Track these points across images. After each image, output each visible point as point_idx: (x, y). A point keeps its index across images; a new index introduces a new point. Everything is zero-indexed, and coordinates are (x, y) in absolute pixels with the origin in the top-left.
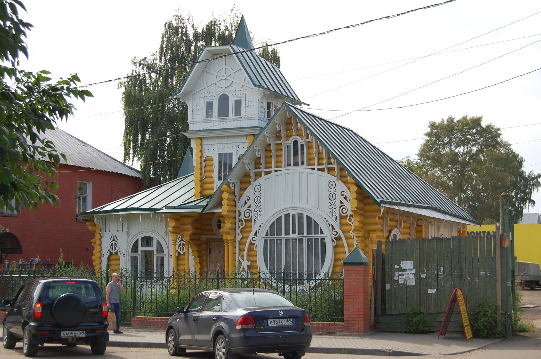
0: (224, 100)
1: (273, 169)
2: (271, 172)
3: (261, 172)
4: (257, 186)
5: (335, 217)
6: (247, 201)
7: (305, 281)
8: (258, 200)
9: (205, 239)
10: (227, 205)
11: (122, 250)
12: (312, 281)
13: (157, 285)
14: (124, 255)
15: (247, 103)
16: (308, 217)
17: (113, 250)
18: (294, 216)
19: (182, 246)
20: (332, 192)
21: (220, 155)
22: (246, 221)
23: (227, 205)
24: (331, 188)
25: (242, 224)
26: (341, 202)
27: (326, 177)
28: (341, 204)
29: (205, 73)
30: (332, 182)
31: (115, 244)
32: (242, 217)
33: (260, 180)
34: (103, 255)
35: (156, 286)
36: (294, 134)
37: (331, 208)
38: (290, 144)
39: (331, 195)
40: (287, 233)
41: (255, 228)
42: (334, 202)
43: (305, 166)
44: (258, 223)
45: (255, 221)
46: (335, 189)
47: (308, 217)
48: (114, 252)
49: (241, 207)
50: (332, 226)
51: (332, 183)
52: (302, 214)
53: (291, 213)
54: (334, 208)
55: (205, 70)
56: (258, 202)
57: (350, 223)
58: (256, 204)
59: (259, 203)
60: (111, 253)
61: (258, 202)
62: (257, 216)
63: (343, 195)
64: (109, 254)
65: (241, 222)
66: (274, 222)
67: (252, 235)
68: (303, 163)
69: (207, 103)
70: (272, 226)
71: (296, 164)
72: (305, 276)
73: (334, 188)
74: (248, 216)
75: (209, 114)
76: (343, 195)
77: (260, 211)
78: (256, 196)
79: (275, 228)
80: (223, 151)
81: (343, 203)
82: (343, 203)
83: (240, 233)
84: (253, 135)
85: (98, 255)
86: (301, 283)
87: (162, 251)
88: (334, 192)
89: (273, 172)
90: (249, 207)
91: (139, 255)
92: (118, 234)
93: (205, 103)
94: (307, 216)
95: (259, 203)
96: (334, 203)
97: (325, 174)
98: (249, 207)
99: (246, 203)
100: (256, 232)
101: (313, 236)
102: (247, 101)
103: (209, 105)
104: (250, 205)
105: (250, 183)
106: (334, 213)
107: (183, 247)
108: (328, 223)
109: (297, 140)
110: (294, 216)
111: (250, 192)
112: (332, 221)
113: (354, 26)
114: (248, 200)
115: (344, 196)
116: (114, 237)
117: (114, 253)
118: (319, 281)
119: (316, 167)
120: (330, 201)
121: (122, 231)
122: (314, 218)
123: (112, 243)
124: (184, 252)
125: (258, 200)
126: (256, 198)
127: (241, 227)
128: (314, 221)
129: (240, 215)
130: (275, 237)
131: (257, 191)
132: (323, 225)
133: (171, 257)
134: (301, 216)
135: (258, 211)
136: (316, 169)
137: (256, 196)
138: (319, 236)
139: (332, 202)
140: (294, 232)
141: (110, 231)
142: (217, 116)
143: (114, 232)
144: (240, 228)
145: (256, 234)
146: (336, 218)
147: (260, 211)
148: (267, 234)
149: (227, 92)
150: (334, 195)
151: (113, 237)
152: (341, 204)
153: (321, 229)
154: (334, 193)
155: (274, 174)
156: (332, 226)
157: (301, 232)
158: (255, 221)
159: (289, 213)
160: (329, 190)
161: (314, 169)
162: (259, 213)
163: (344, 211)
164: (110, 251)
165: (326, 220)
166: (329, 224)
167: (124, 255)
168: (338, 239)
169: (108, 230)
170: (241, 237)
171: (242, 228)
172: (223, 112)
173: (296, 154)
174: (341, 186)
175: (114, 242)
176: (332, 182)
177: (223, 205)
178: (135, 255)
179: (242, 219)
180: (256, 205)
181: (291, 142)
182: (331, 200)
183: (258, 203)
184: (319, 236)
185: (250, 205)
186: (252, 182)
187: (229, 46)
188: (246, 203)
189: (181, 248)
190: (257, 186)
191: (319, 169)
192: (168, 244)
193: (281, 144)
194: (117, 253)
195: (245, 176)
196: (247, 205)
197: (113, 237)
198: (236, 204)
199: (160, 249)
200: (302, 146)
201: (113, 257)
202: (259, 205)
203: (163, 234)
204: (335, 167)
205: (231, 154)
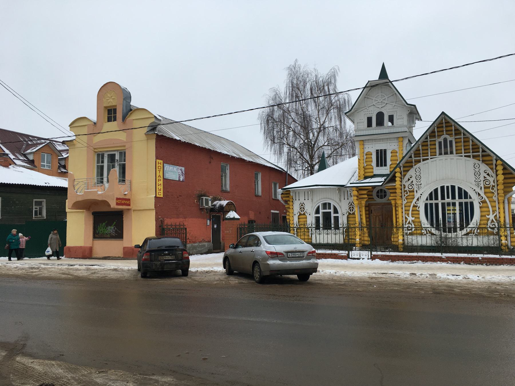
0: (380, 116)
1: (429, 157)
2: (428, 159)
3: (420, 159)
5: (481, 187)
6: (410, 178)
8: (478, 174)
9: (368, 204)
10: (502, 174)
13: (339, 233)
14: (310, 214)
17: (301, 211)
18: (448, 187)
19: (351, 208)
20: (477, 171)
21: (377, 151)
22: (410, 192)
23: (502, 174)
24: (476, 168)
26: (485, 177)
27: (471, 161)
28: (484, 178)
29: (366, 98)
32: (407, 189)
33: (419, 165)
34: (295, 215)
36: (445, 133)
37: (477, 182)
40: (443, 198)
41: (417, 196)
42: (479, 177)
43: (455, 154)
44: (420, 192)
45: (417, 191)
46: (479, 168)
48: (351, 212)
51: (477, 165)
53: (445, 185)
54: (479, 182)
56: (418, 179)
57: (493, 191)
58: (417, 180)
59: (479, 176)
60: (350, 214)
61: (477, 175)
62: (418, 188)
64: (348, 214)
67: (415, 200)
69: (368, 118)
70: (431, 194)
71: (446, 153)
72: (458, 226)
78: (475, 171)
79: (434, 195)
80: (379, 148)
81: (486, 178)
82: (486, 178)
83: (405, 199)
85: (291, 215)
86: (455, 231)
89: (429, 159)
90: (412, 182)
91: (320, 215)
93: (388, 116)
95: (479, 176)
97: (471, 159)
98: (412, 182)
99: (409, 180)
100: (418, 199)
101: (463, 200)
102: (398, 115)
103: (369, 120)
106: (479, 185)
110: (448, 187)
111: (412, 172)
112: (478, 190)
115: (487, 173)
116: (351, 203)
117: (351, 213)
118: (470, 229)
119: (463, 154)
120: (475, 177)
122: (464, 188)
123: (301, 207)
126: (417, 177)
127: (406, 195)
128: (464, 190)
129: (404, 188)
130: (434, 202)
131: (418, 172)
132: (471, 193)
134: (453, 187)
136: (463, 156)
137: (475, 171)
138: (468, 200)
140: (448, 198)
141: (299, 200)
142: (367, 127)
143: (302, 200)
144: (405, 196)
145: (418, 199)
146: (481, 188)
147: (420, 185)
148: (427, 200)
149: (383, 110)
150: (478, 173)
151: (301, 204)
152: (484, 178)
153: (470, 195)
155: (430, 160)
157: (454, 197)
158: (417, 191)
161: (462, 156)
162: (420, 186)
163: (487, 183)
166: (476, 192)
167: (310, 214)
168: (484, 202)
169: (297, 199)
172: (380, 122)
173: (446, 146)
174: (484, 167)
175: (302, 207)
177: (396, 181)
179: (406, 190)
180: (417, 181)
181: (441, 139)
182: (477, 176)
184: (468, 200)
186: (413, 166)
188: (409, 180)
189: (351, 209)
191: (465, 156)
196: (410, 181)
197: (301, 204)
198: (402, 180)
199: (336, 211)
200: (451, 142)
201: (302, 215)
202: (420, 180)
203: (338, 200)
204: (480, 155)
205: (385, 151)
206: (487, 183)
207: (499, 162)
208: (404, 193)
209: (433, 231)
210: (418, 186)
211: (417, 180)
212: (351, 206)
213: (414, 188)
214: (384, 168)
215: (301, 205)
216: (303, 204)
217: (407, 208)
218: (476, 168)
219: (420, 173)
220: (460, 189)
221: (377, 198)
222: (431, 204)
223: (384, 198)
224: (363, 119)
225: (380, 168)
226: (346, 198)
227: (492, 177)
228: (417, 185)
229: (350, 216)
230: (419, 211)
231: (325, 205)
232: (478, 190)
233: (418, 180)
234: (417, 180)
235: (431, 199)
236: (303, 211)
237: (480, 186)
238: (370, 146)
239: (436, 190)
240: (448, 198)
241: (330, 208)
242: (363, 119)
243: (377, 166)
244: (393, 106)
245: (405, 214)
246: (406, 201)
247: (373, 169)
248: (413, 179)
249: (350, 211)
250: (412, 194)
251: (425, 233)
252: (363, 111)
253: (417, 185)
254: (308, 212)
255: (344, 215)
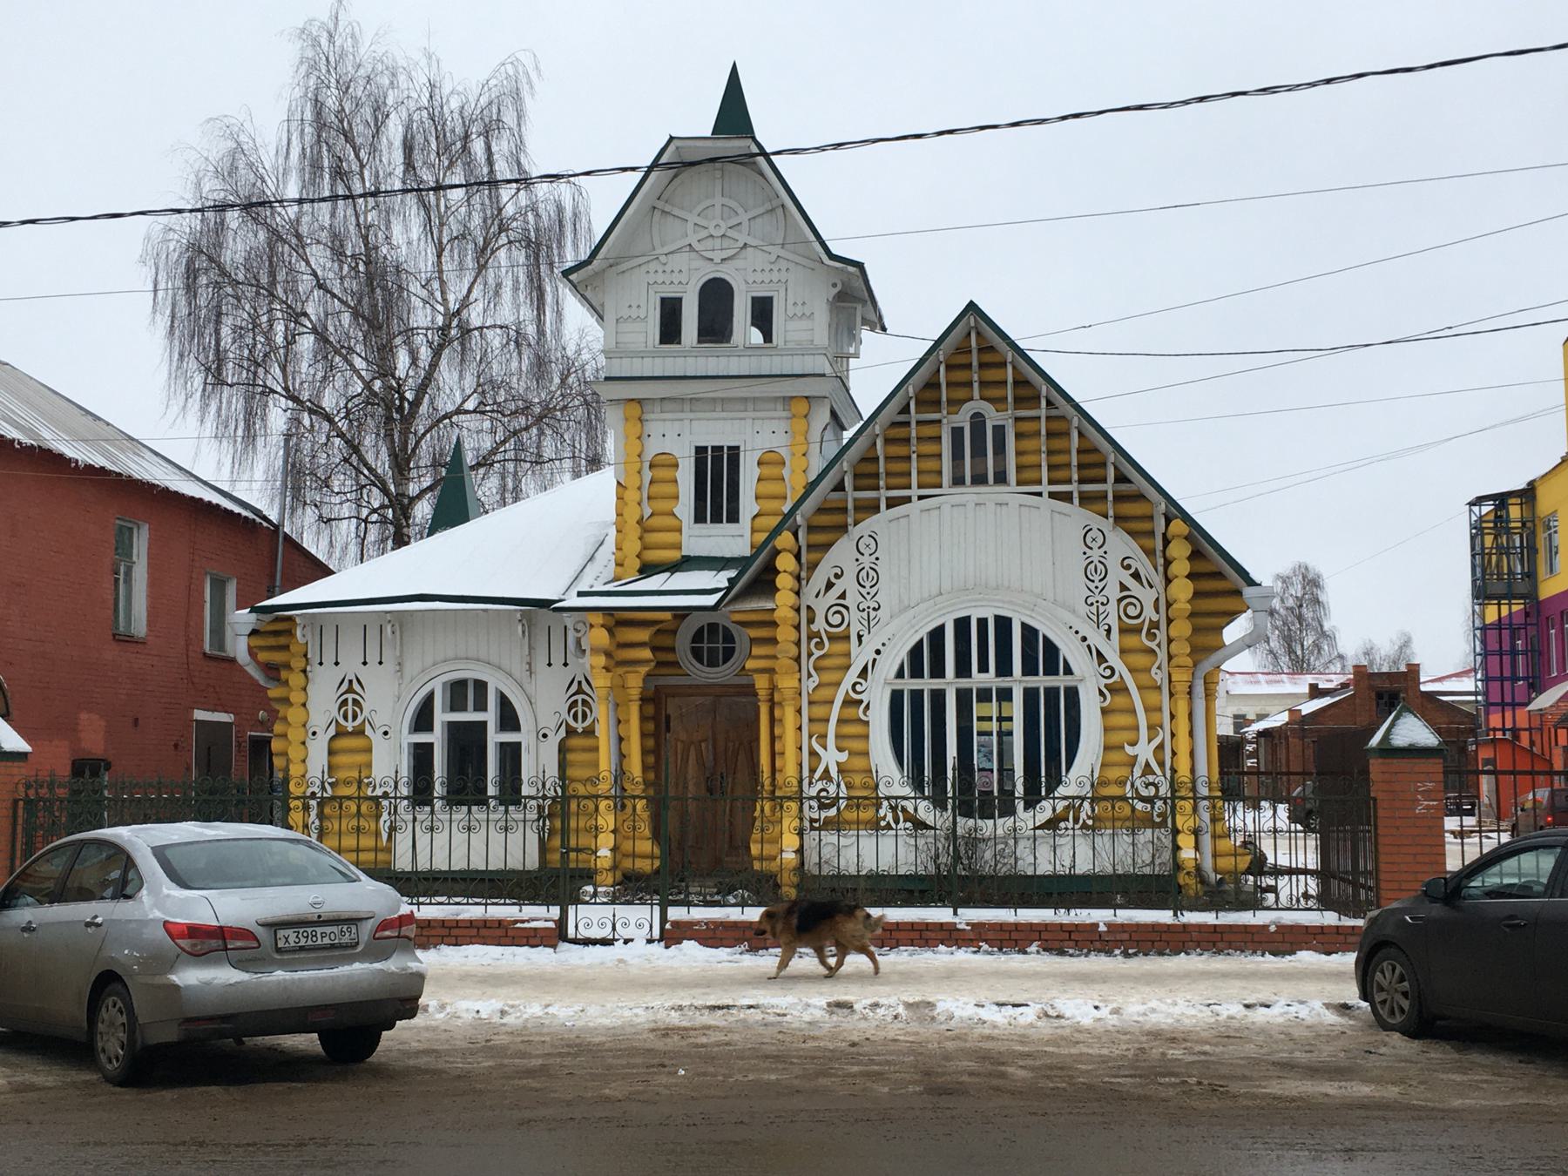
0: (716, 296)
1: (914, 492)
2: (908, 500)
4: (866, 537)
5: (1107, 627)
7: (1020, 805)
8: (870, 579)
11: (377, 722)
12: (1044, 803)
14: (386, 733)
15: (790, 306)
16: (1024, 626)
17: (346, 718)
18: (982, 623)
19: (580, 708)
20: (1096, 559)
21: (700, 451)
22: (832, 638)
24: (1091, 548)
25: (820, 645)
26: (1123, 587)
27: (1076, 517)
28: (1121, 591)
29: (657, 214)
30: (1095, 529)
31: (355, 702)
32: (819, 625)
33: (872, 523)
35: (447, 825)
36: (976, 394)
38: (960, 425)
39: (1092, 567)
40: (963, 670)
41: (860, 656)
42: (1101, 585)
44: (871, 643)
45: (860, 637)
47: (1024, 626)
48: (580, 726)
49: (817, 596)
50: (1099, 653)
52: (1010, 620)
54: (1102, 604)
55: (660, 204)
56: (868, 584)
57: (1153, 645)
59: (871, 587)
60: (571, 732)
61: (868, 584)
62: (866, 623)
63: (1128, 567)
65: (818, 640)
66: (922, 640)
67: (852, 676)
68: (1001, 478)
70: (916, 652)
71: (979, 479)
73: (1099, 548)
74: (834, 623)
75: (670, 331)
76: (1128, 567)
77: (874, 609)
80: (709, 441)
81: (1129, 590)
84: (806, 397)
85: (294, 735)
86: (1008, 811)
87: (516, 727)
88: (1102, 559)
89: (915, 499)
90: (843, 596)
91: (436, 738)
92: (363, 674)
94: (1023, 625)
95: (871, 587)
96: (1100, 588)
98: (843, 596)
99: (830, 585)
100: (865, 668)
101: (1041, 681)
102: (790, 302)
103: (670, 312)
104: (845, 592)
105: (843, 529)
106: (1101, 618)
107: (354, 711)
108: (1086, 643)
109: (976, 411)
110: (982, 623)
111: (842, 553)
112: (1097, 639)
113: (1244, 93)
114: (837, 576)
115: (1132, 570)
116: (580, 683)
117: (580, 730)
119: (1045, 488)
121: (550, 665)
122: (1044, 629)
124: (587, 723)
125: (870, 579)
126: (863, 573)
127: (817, 653)
129: (811, 621)
130: (927, 684)
131: (867, 552)
132: (1070, 651)
133: (542, 739)
134: (1003, 624)
135: (871, 610)
136: (1045, 495)
138: (1060, 681)
139: (1097, 587)
140: (983, 668)
141: (337, 664)
143: (351, 665)
144: (813, 659)
146: (1109, 631)
147: (874, 609)
148: (900, 674)
149: (727, 273)
150: (1100, 567)
151: (575, 683)
152: (1121, 591)
153: (1065, 660)
154: (1100, 562)
155: (915, 503)
156: (1098, 652)
157: (1004, 669)
158: (860, 637)
159: (969, 617)
160: (1085, 553)
161: (1039, 494)
162: (873, 614)
164: (567, 724)
165: (1080, 635)
166: (1089, 647)
167: (386, 733)
168: (1118, 689)
169: (329, 658)
170: (816, 684)
171: (819, 658)
172: (715, 328)
173: (978, 451)
175: (350, 696)
176: (1095, 529)
177: (778, 590)
178: (423, 738)
180: (864, 591)
181: (963, 418)
182: (1093, 581)
183: (868, 587)
184: (1060, 681)
185: (845, 592)
187: (750, 140)
188: (830, 585)
189: (346, 711)
190: (866, 537)
191: (1052, 495)
192: (533, 701)
193: (939, 421)
194: (359, 732)
195: (819, 509)
197: (575, 683)
199: (509, 720)
200: (999, 431)
205: (734, 452)
206: (1132, 611)
207: (1178, 526)
208: (809, 643)
209: (925, 811)
210: (865, 615)
211: (864, 587)
212: (579, 697)
213: (849, 625)
214: (726, 527)
215: (574, 688)
216: (584, 684)
217: (819, 711)
218: (1091, 548)
219: (877, 559)
220: (1029, 633)
221: (694, 662)
222: (917, 696)
223: (724, 662)
224: (643, 305)
225: (709, 528)
226: (557, 659)
227: (1151, 587)
228: (864, 610)
229: (574, 742)
230: (867, 723)
231: (458, 692)
232: (1097, 639)
233: (868, 589)
234: (864, 587)
235: (917, 672)
236: (585, 717)
237: (1104, 622)
238: (671, 428)
239: (937, 635)
240: (983, 668)
241: (481, 706)
242: (643, 305)
243: (699, 518)
244: (773, 258)
245: (810, 737)
246: (816, 679)
247: (680, 531)
248: (847, 583)
249: (575, 718)
250: (839, 647)
251: (890, 817)
252: (644, 268)
253: (864, 610)
254: (377, 724)
255: (545, 736)
